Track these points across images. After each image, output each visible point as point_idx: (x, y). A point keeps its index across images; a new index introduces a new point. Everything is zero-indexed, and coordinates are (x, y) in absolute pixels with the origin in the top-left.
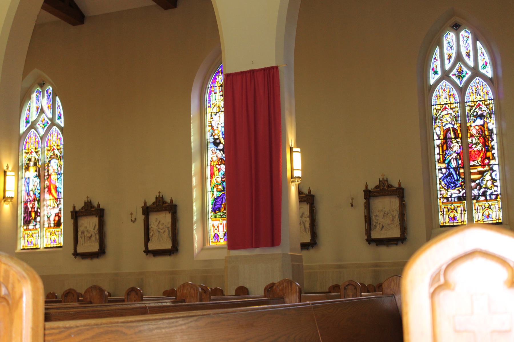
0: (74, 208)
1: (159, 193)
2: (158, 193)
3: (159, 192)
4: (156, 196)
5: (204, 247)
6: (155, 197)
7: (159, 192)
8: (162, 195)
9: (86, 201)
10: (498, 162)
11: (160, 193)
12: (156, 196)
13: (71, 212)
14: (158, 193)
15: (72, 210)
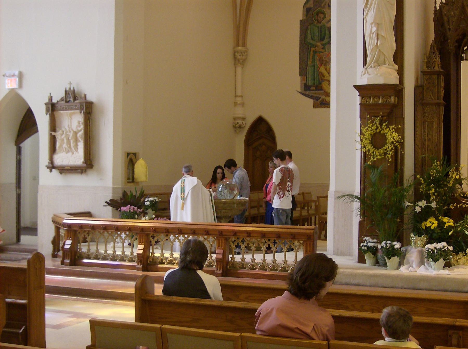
0: (51, 99)
1: (70, 83)
2: (69, 84)
3: (70, 82)
4: (66, 88)
5: (423, 101)
6: (65, 89)
7: (70, 82)
8: (74, 88)
9: (67, 89)
10: (195, 177)
11: (71, 84)
12: (66, 88)
13: (46, 104)
14: (69, 84)
15: (47, 101)
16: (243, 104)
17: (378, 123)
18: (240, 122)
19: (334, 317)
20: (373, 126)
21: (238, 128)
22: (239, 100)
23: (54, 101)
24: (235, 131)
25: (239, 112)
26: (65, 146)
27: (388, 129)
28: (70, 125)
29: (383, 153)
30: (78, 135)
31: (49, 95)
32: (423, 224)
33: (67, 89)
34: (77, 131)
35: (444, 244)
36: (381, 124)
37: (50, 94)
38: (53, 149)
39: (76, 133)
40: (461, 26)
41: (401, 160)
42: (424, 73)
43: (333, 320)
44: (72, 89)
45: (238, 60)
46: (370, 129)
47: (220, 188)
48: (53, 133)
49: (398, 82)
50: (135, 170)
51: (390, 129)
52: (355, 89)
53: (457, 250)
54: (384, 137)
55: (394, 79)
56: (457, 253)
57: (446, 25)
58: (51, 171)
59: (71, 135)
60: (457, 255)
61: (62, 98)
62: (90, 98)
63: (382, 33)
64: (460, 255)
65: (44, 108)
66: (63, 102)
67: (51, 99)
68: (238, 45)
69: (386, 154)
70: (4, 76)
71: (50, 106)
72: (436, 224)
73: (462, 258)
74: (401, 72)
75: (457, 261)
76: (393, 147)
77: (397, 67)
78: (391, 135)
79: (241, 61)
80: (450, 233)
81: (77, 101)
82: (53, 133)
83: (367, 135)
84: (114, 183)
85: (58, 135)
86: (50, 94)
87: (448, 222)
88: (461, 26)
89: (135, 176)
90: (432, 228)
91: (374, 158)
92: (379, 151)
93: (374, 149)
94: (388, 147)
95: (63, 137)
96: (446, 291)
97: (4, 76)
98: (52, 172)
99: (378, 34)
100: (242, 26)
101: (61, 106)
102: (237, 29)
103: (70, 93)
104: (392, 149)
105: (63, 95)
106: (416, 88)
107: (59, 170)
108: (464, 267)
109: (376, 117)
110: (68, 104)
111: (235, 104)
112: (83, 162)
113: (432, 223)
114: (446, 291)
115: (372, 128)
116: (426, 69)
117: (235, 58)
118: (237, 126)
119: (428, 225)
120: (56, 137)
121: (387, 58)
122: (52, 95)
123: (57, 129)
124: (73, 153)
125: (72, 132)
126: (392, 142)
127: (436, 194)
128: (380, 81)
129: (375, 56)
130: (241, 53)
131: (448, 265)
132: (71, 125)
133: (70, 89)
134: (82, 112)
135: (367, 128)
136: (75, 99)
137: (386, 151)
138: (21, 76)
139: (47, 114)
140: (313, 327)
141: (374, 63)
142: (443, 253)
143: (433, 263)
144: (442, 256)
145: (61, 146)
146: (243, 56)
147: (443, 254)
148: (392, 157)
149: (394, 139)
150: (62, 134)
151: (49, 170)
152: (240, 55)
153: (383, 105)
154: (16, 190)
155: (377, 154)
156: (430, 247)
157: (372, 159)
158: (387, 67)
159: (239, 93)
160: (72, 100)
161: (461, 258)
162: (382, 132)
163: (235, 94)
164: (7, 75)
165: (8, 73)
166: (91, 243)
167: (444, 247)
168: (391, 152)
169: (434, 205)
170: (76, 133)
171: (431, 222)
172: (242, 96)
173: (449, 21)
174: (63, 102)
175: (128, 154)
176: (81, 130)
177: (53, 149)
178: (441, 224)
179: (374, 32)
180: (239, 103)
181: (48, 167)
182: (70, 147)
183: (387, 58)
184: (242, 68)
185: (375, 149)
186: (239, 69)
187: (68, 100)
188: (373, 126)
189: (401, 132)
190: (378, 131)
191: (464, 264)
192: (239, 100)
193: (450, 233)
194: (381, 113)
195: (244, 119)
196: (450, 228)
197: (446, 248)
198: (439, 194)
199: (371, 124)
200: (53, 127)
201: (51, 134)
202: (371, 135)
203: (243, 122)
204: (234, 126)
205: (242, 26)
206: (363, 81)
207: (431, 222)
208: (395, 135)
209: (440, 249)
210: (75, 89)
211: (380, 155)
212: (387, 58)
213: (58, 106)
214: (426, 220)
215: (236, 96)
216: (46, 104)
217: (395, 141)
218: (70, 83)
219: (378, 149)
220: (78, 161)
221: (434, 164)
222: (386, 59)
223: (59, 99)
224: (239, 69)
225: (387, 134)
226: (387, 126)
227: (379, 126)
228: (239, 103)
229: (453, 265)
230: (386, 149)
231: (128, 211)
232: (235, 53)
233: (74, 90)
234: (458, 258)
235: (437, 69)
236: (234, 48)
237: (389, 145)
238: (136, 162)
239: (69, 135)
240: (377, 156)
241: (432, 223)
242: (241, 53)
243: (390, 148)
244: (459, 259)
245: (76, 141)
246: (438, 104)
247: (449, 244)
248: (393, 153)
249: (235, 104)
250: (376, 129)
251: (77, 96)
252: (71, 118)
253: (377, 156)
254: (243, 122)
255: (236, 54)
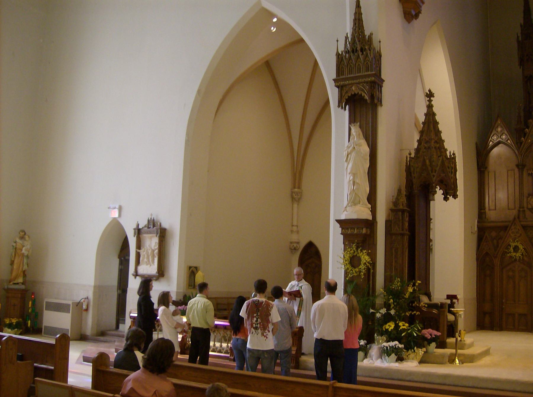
0: (138, 225)
1: (152, 215)
4: (148, 218)
6: (148, 219)
8: (154, 218)
9: (149, 219)
12: (148, 218)
15: (135, 227)
16: (298, 232)
17: (354, 249)
18: (295, 245)
19: (175, 385)
20: (351, 250)
21: (294, 250)
22: (295, 228)
23: (140, 227)
24: (292, 252)
25: (294, 237)
26: (145, 260)
27: (362, 253)
28: (150, 245)
29: (358, 271)
30: (155, 252)
31: (137, 222)
32: (384, 327)
33: (149, 219)
34: (154, 249)
35: (397, 342)
36: (357, 249)
37: (138, 222)
38: (138, 262)
39: (153, 251)
40: (422, 174)
41: (373, 276)
42: (392, 210)
43: (174, 388)
44: (152, 218)
45: (295, 199)
46: (349, 253)
47: (253, 295)
48: (138, 251)
49: (370, 218)
50: (196, 279)
51: (363, 253)
52: (336, 222)
53: (408, 347)
54: (360, 259)
55: (366, 214)
56: (408, 350)
57: (412, 174)
58: (135, 278)
59: (150, 252)
60: (407, 352)
61: (146, 225)
62: (165, 225)
63: (357, 181)
64: (410, 351)
65: (133, 231)
66: (146, 228)
67: (138, 225)
68: (295, 188)
69: (360, 272)
70: (109, 208)
71: (137, 231)
72: (393, 326)
73: (411, 354)
74: (374, 211)
75: (408, 356)
76: (366, 266)
77: (370, 206)
78: (364, 257)
79: (297, 200)
80: (403, 334)
81: (155, 228)
82: (138, 251)
83: (347, 257)
84: (178, 288)
85: (142, 252)
86: (138, 222)
87: (403, 325)
88: (422, 174)
89: (195, 284)
90: (390, 330)
91: (351, 275)
92: (355, 270)
93: (352, 268)
94: (362, 267)
95: (144, 253)
96: (393, 379)
97: (109, 208)
98: (136, 279)
99: (354, 182)
100: (297, 175)
101: (144, 231)
102: (294, 175)
103: (151, 222)
104: (365, 268)
105: (146, 223)
106: (387, 222)
107: (141, 277)
108: (413, 361)
109: (353, 243)
110: (149, 229)
111: (292, 231)
112: (156, 272)
113: (390, 326)
114: (393, 379)
115: (351, 252)
116: (393, 208)
117: (292, 198)
118: (293, 248)
119: (387, 327)
120: (140, 253)
121: (362, 200)
122: (139, 223)
123: (141, 247)
124: (151, 265)
125: (151, 250)
126: (365, 263)
127: (395, 304)
128: (354, 217)
129: (352, 198)
130: (297, 193)
131: (400, 359)
132: (151, 245)
133: (151, 218)
134: (158, 236)
135: (346, 252)
136: (154, 226)
137: (360, 270)
138: (120, 209)
139: (134, 236)
140: (155, 391)
141: (352, 202)
142: (395, 350)
143: (387, 357)
144: (393, 352)
145: (143, 260)
146: (298, 195)
147: (395, 350)
148: (364, 274)
149: (366, 261)
150: (144, 251)
151: (134, 277)
152: (296, 195)
153: (357, 235)
154: (118, 291)
155: (354, 272)
156: (385, 345)
157: (350, 275)
158: (360, 206)
159: (295, 223)
160: (152, 226)
161: (410, 354)
162: (358, 255)
163: (292, 224)
164: (112, 207)
165: (112, 206)
166: (159, 332)
167: (395, 345)
168: (364, 271)
169: (393, 312)
170: (153, 251)
171: (389, 326)
172: (297, 226)
173: (414, 171)
174: (146, 228)
175: (190, 267)
176: (156, 249)
177: (138, 262)
178: (397, 326)
179: (351, 180)
180: (294, 231)
181: (133, 275)
182: (149, 261)
183: (361, 199)
184: (298, 205)
185: (353, 268)
186: (295, 205)
187: (150, 226)
188: (351, 250)
189: (373, 256)
190: (355, 254)
191: (413, 359)
192: (295, 228)
193: (403, 334)
194: (356, 241)
195: (298, 243)
196: (404, 330)
197: (397, 346)
198: (398, 304)
199: (350, 249)
200: (139, 246)
201: (136, 251)
202: (350, 257)
203: (298, 245)
204: (290, 248)
205: (297, 175)
206: (343, 217)
207: (389, 326)
208: (367, 258)
209: (393, 347)
210: (155, 219)
211: (356, 273)
212: (362, 200)
213: (142, 231)
214: (386, 324)
215: (293, 226)
216: (134, 229)
217: (367, 262)
218: (152, 215)
219: (355, 268)
220: (154, 271)
221: (396, 280)
222: (361, 200)
223: (143, 226)
224: (295, 205)
225: (361, 256)
226: (361, 251)
227: (355, 250)
228: (294, 231)
229: (404, 359)
230: (361, 268)
231: (182, 309)
232: (292, 193)
233: (154, 220)
234: (408, 354)
235: (401, 207)
236: (291, 190)
237: (363, 265)
238: (196, 274)
239: (149, 252)
240: (353, 273)
241: (390, 326)
242: (297, 193)
243: (363, 268)
244: (409, 355)
245: (153, 256)
246: (402, 235)
247: (400, 343)
248: (366, 271)
249: (292, 231)
250: (354, 253)
251: (156, 224)
252: (151, 240)
253: (353, 273)
254: (298, 245)
255: (293, 194)
